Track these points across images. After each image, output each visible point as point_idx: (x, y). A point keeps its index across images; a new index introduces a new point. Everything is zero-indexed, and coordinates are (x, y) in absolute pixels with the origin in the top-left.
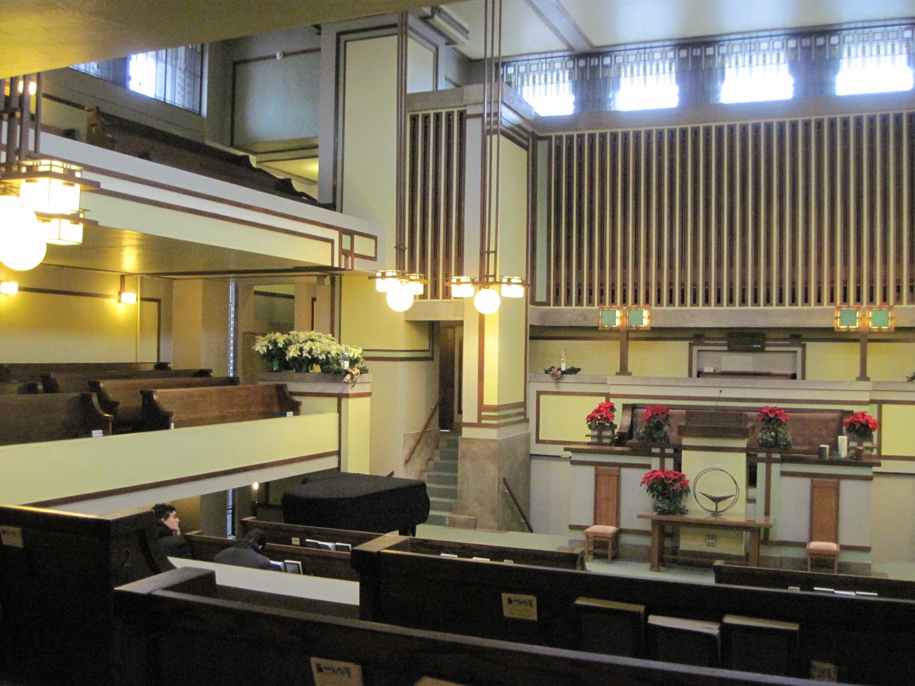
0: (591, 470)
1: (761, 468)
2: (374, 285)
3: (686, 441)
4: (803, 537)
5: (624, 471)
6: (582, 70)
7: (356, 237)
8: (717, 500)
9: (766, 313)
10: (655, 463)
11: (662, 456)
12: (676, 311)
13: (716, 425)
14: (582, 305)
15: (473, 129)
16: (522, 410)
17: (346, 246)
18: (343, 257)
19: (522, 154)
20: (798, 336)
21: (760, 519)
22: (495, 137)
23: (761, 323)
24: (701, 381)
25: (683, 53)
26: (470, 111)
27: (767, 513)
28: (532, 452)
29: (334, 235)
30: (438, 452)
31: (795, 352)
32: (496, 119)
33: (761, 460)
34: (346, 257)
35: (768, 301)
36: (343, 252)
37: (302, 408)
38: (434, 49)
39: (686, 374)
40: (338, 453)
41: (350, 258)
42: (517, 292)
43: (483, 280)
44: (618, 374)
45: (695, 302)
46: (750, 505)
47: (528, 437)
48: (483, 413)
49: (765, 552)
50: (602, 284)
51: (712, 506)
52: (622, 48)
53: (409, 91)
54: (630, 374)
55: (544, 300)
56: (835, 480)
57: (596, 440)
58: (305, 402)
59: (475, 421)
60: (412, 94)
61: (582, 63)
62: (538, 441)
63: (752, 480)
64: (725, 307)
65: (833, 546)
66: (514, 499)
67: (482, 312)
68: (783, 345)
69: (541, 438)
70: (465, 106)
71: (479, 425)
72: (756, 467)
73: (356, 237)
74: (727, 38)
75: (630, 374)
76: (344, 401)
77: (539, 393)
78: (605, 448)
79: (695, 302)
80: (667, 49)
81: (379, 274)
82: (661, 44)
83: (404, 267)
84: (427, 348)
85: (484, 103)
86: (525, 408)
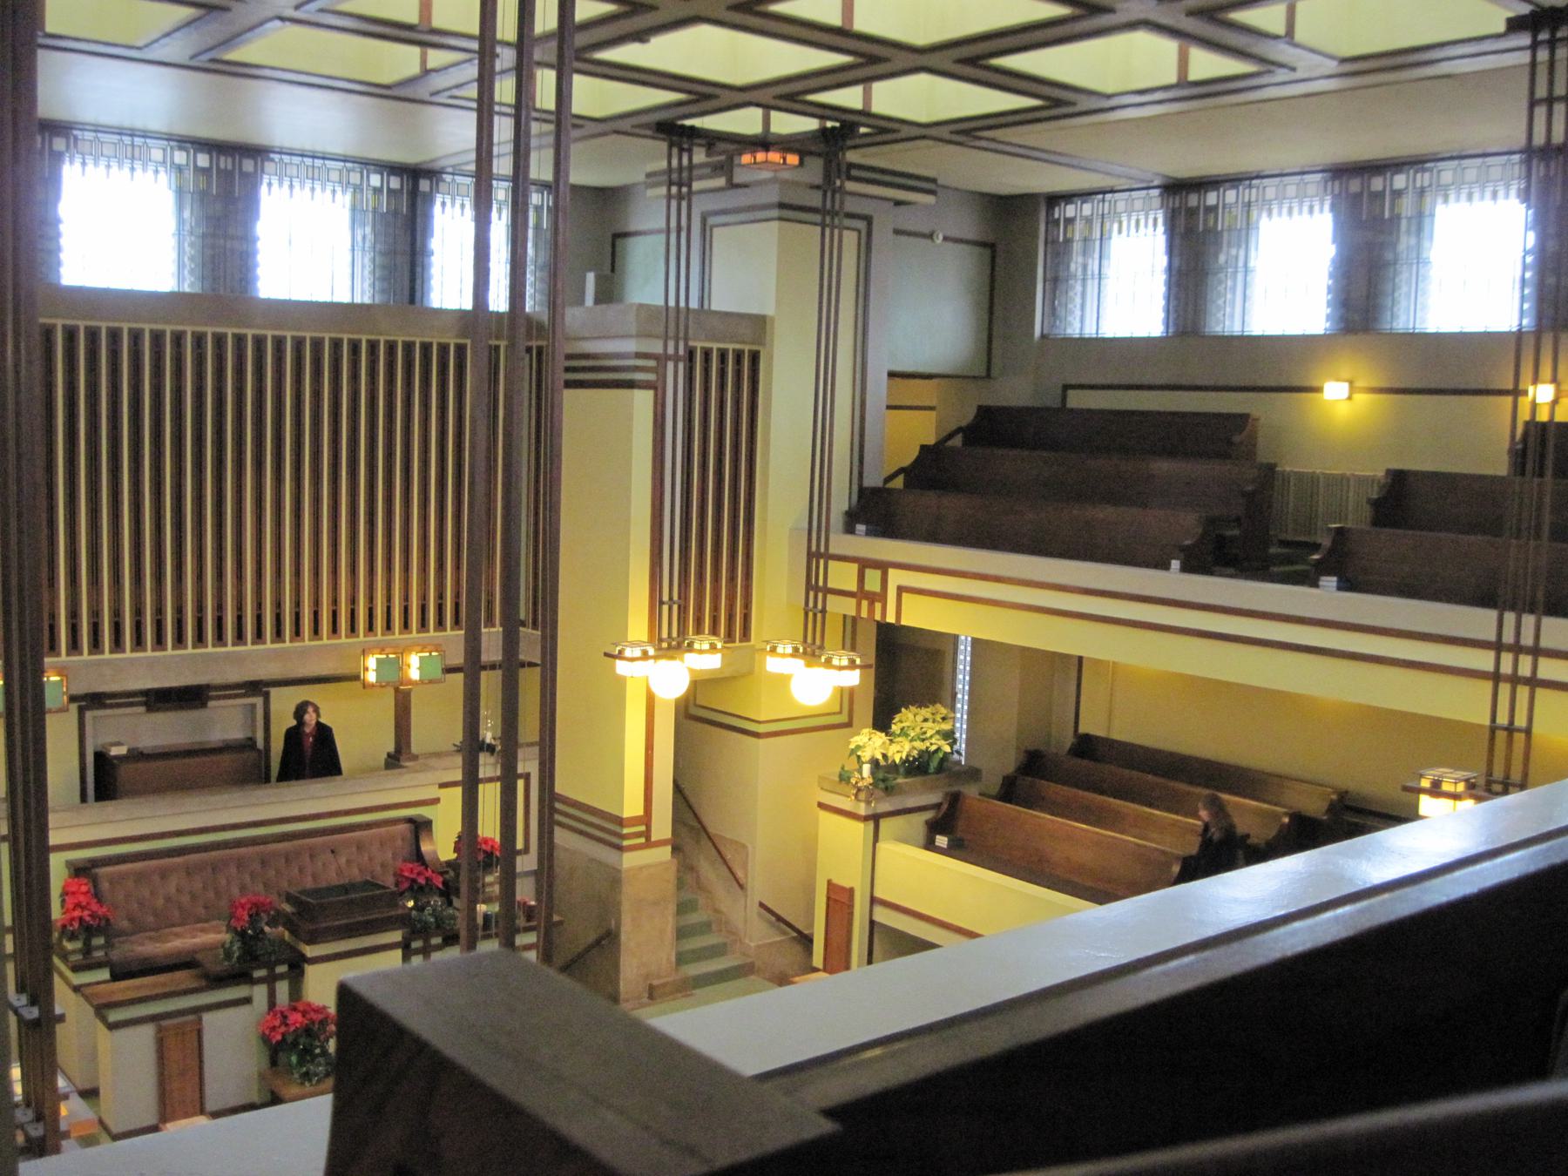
0: (147, 1032)
2: (613, 668)
3: (310, 951)
5: (207, 1018)
10: (260, 993)
11: (271, 980)
14: (124, 651)
45: (117, 644)
79: (117, 644)
81: (1425, 783)
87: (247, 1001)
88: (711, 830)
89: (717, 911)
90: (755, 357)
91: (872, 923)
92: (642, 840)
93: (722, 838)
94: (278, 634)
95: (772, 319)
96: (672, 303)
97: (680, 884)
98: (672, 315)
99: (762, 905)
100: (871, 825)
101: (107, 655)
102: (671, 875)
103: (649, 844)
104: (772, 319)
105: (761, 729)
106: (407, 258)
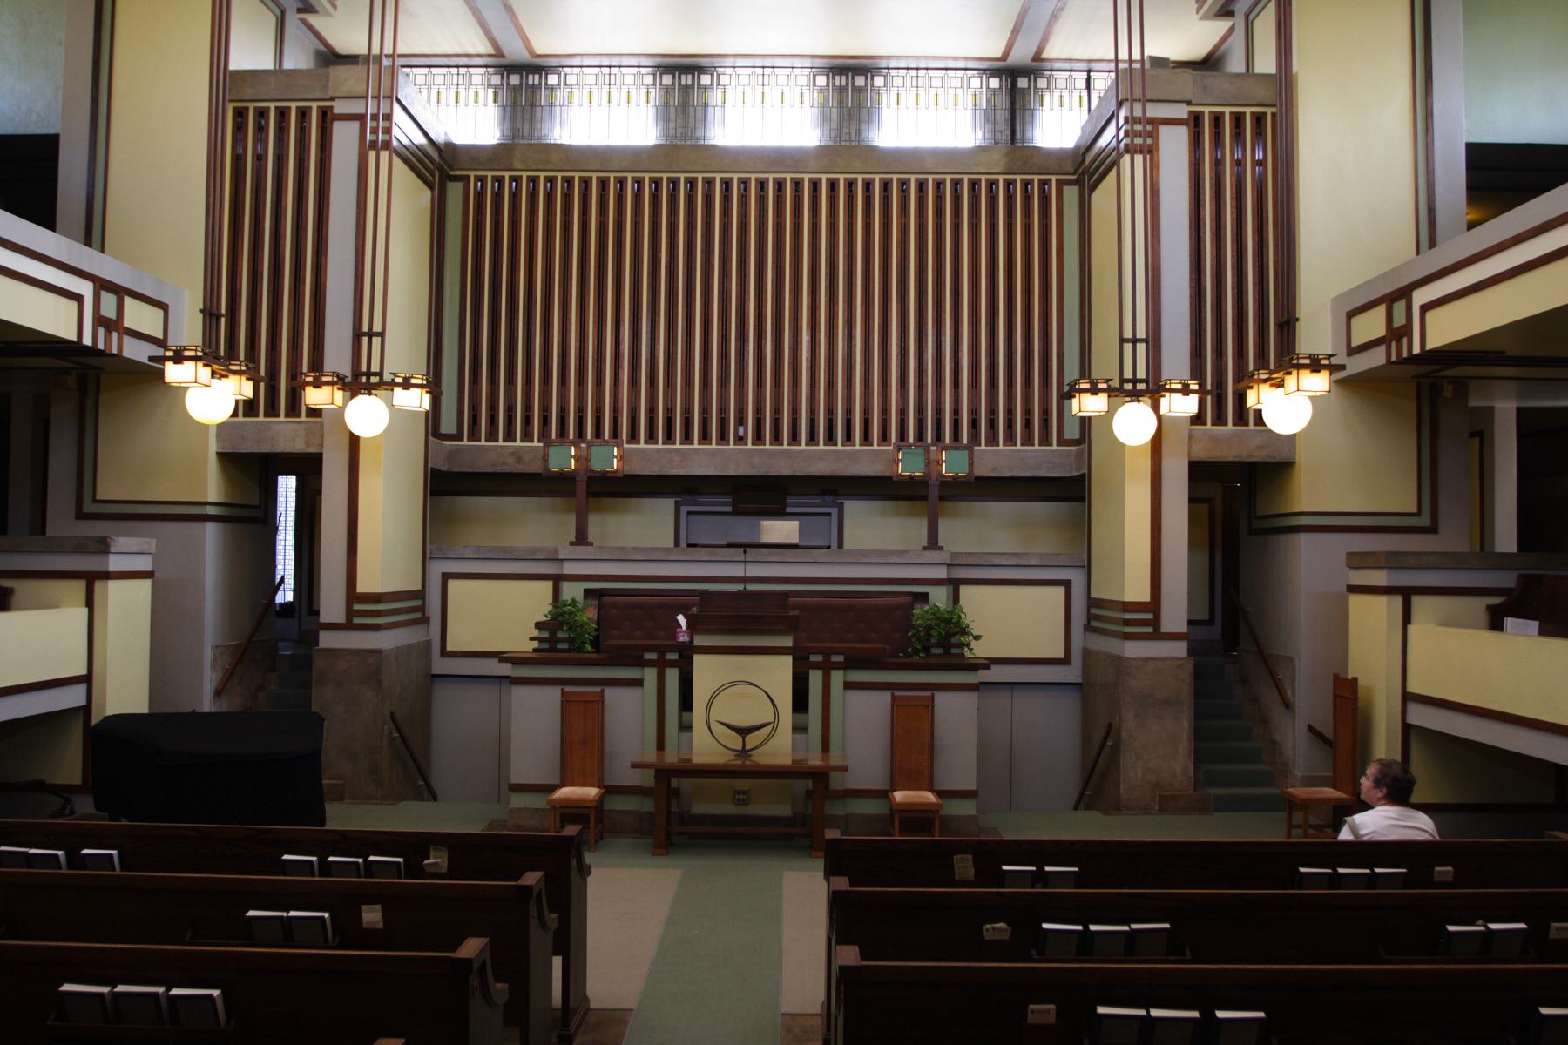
1: (815, 678)
3: (700, 641)
6: (516, 90)
7: (128, 300)
8: (743, 732)
11: (661, 665)
13: (743, 617)
15: (345, 138)
16: (418, 603)
17: (109, 310)
18: (101, 331)
19: (426, 195)
21: (815, 760)
22: (384, 155)
23: (784, 469)
25: (667, 80)
26: (339, 107)
27: (826, 747)
28: (434, 672)
29: (85, 288)
31: (829, 514)
32: (387, 124)
33: (816, 666)
34: (108, 332)
36: (99, 321)
37: (16, 599)
38: (278, 13)
40: (87, 679)
41: (115, 335)
42: (416, 400)
43: (358, 383)
44: (572, 544)
46: (800, 737)
47: (427, 645)
48: (356, 607)
49: (835, 809)
50: (545, 408)
51: (735, 742)
52: (576, 62)
53: (232, 66)
55: (454, 431)
57: (546, 646)
58: (22, 588)
60: (237, 72)
61: (515, 80)
62: (445, 653)
63: (800, 702)
65: (930, 797)
66: (407, 746)
67: (356, 432)
69: (449, 647)
70: (332, 99)
71: (348, 626)
72: (807, 679)
73: (128, 300)
74: (729, 62)
76: (98, 585)
77: (446, 577)
78: (559, 655)
80: (643, 70)
82: (634, 62)
83: (217, 357)
84: (256, 503)
85: (366, 98)
86: (424, 599)
87: (638, 683)
91: (1407, 729)
92: (1150, 630)
94: (848, 437)
96: (1123, 55)
98: (1137, 77)
99: (1311, 729)
100: (1398, 601)
103: (1158, 635)
105: (1304, 521)
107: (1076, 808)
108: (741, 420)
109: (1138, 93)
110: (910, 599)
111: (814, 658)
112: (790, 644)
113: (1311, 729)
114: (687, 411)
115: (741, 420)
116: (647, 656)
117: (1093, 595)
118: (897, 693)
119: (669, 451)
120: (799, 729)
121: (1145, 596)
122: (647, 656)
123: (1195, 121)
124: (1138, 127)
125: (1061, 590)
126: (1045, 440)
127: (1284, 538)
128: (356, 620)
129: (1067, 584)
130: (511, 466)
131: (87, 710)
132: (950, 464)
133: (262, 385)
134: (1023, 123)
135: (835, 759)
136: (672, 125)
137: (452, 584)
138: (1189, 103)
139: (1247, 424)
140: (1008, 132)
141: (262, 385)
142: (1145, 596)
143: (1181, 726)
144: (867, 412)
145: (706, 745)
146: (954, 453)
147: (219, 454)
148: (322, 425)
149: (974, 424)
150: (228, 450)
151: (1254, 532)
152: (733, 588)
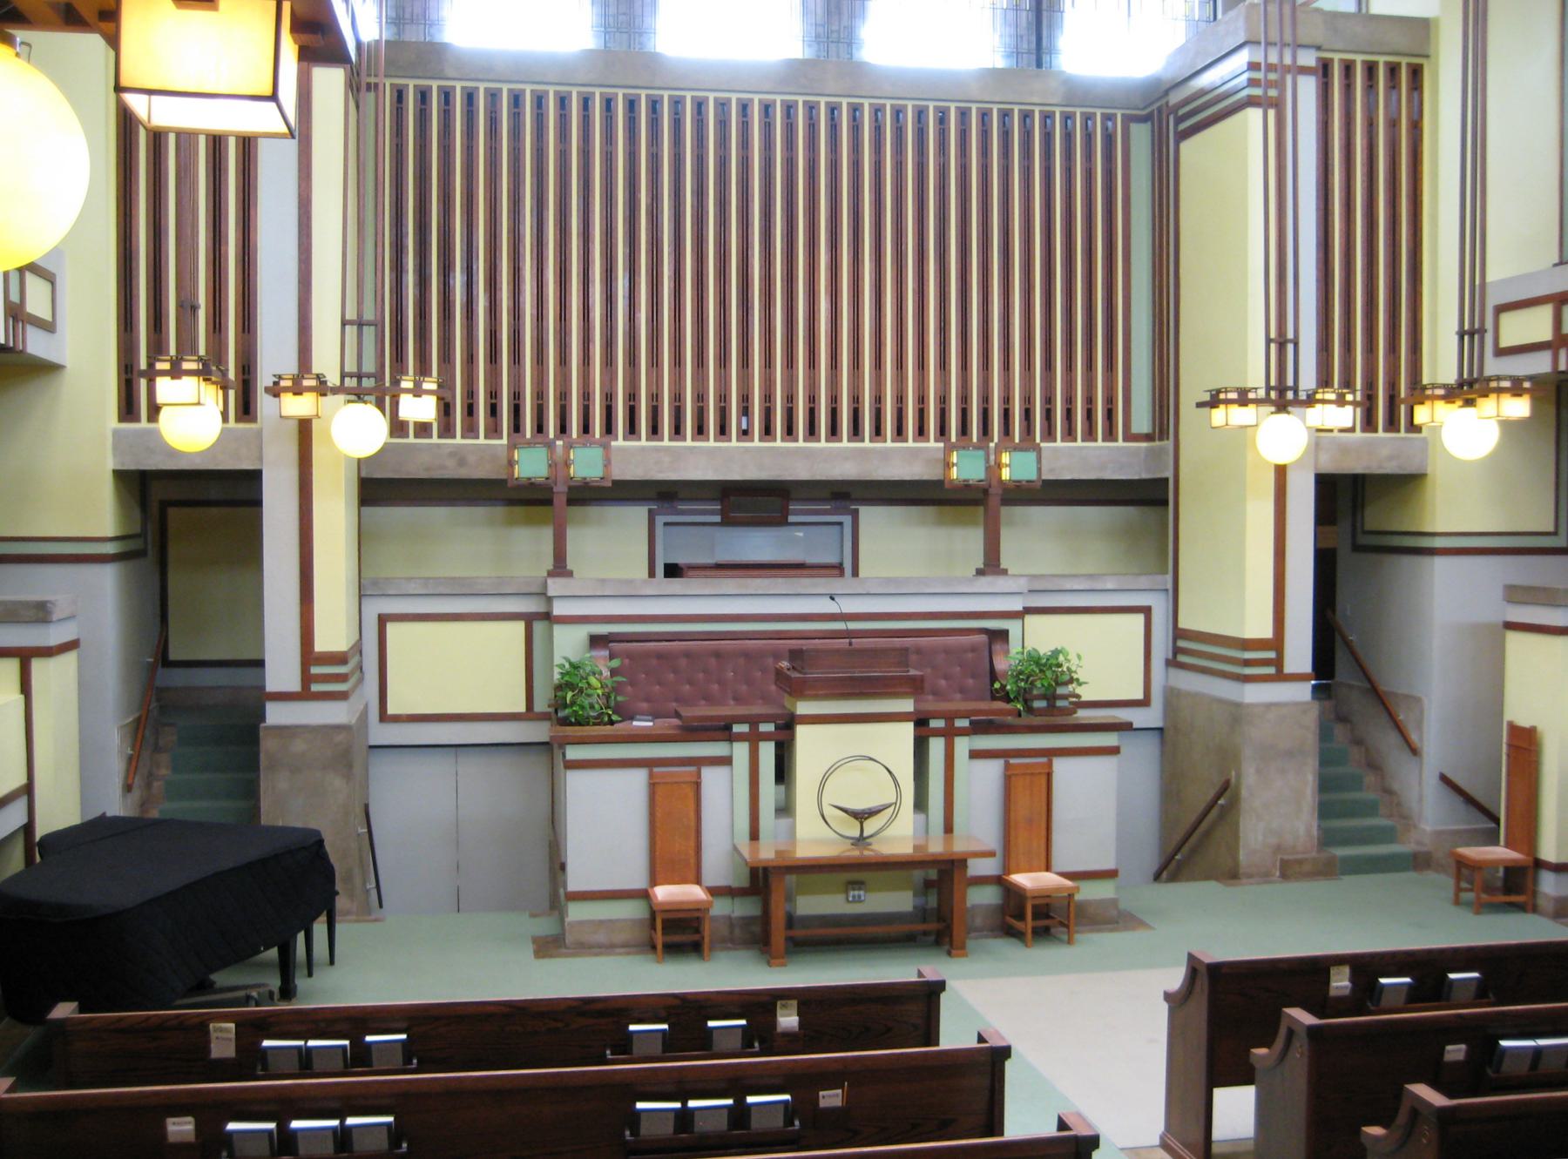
0: (639, 777)
3: (803, 708)
4: (638, 881)
8: (861, 816)
9: (676, 454)
11: (754, 739)
12: (643, 449)
20: (845, 496)
21: (936, 847)
24: (676, 585)
27: (949, 828)
30: (164, 758)
31: (840, 524)
35: (812, 431)
39: (645, 573)
40: (28, 790)
48: (315, 670)
54: (1005, 572)
56: (693, 769)
59: (294, 685)
64: (845, 443)
68: (825, 513)
69: (391, 710)
71: (305, 695)
75: (1005, 572)
87: (726, 761)
88: (1383, 688)
89: (1388, 791)
90: (1416, 72)
92: (1271, 670)
93: (1396, 695)
95: (1436, 20)
97: (1325, 734)
99: (1444, 779)
101: (666, 443)
102: (1311, 718)
103: (1281, 677)
104: (1436, 20)
105: (1439, 543)
106: (1032, 16)
107: (1157, 877)
108: (745, 411)
109: (1288, 38)
110: (984, 638)
111: (934, 724)
112: (911, 709)
113: (1444, 779)
114: (677, 398)
115: (745, 411)
116: (737, 728)
117: (1181, 625)
118: (1012, 761)
119: (657, 449)
120: (920, 804)
121: (1267, 632)
122: (737, 728)
123: (1325, 68)
124: (1259, 75)
125: (1139, 619)
126: (1110, 434)
127: (1406, 560)
128: (315, 688)
129: (1146, 611)
130: (452, 471)
131: (28, 828)
132: (1015, 467)
133: (232, 393)
134: (1050, 26)
135: (959, 846)
136: (612, 10)
137: (391, 628)
138: (1319, 48)
139: (1376, 431)
140: (1034, 39)
141: (232, 393)
142: (1267, 632)
143: (1306, 780)
144: (900, 399)
145: (813, 834)
146: (1019, 455)
147: (115, 472)
148: (259, 433)
149: (1028, 414)
150: (131, 465)
151: (1358, 548)
152: (843, 643)
